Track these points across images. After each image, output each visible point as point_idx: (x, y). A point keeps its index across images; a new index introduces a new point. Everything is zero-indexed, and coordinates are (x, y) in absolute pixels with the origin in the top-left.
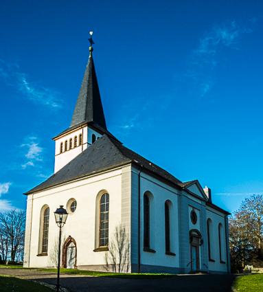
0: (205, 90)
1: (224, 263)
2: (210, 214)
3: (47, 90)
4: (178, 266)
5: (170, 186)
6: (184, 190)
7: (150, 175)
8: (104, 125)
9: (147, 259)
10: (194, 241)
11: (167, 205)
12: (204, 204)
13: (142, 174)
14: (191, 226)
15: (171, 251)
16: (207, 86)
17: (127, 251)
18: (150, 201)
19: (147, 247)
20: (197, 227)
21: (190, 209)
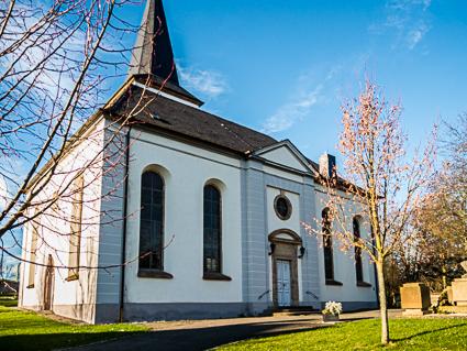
0: (416, 40)
1: (369, 286)
2: (328, 198)
3: (204, 73)
4: (240, 300)
5: (205, 149)
6: (252, 159)
7: (162, 135)
8: (174, 79)
9: (143, 291)
10: (282, 250)
11: (212, 193)
12: (311, 182)
13: (134, 133)
14: (275, 223)
15: (337, 278)
16: (419, 34)
17: (94, 279)
18: (223, 194)
19: (152, 264)
20: (293, 224)
21: (273, 194)
